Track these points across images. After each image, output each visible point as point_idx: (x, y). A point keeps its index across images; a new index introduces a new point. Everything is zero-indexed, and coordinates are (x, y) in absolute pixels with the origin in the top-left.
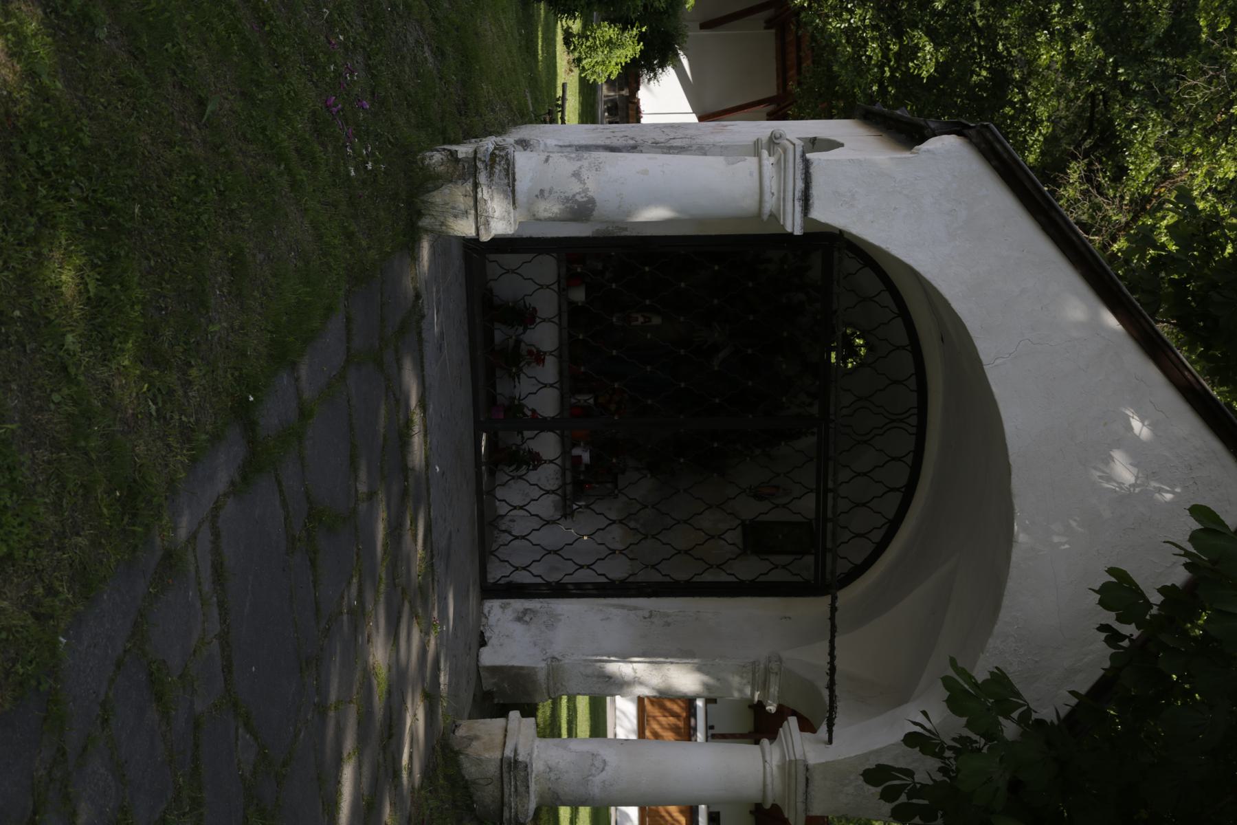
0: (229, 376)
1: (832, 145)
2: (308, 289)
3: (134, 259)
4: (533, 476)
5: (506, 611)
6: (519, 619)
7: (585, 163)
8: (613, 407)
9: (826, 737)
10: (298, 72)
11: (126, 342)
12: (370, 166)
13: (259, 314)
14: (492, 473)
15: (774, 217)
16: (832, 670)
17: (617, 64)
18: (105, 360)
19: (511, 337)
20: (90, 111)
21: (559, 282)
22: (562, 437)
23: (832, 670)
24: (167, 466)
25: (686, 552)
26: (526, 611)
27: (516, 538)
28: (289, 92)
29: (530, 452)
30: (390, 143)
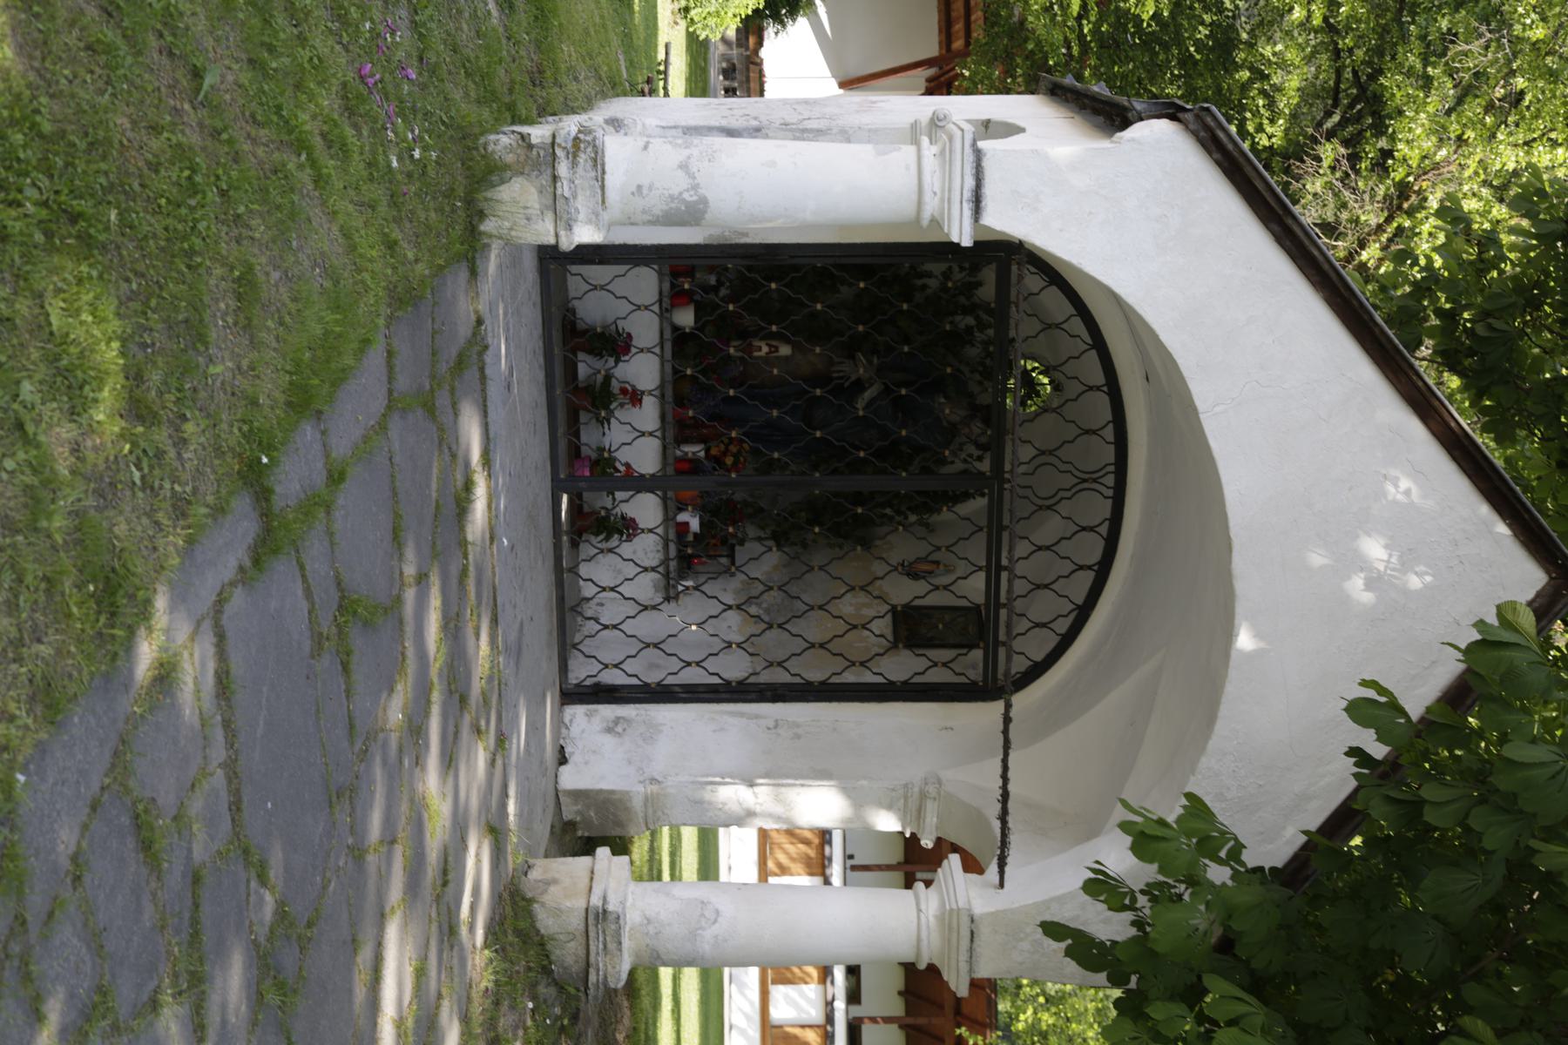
0: (236, 430)
1: (1010, 130)
2: (338, 316)
3: (110, 281)
4: (626, 549)
5: (593, 719)
6: (609, 730)
7: (695, 152)
8: (729, 461)
9: (996, 879)
10: (323, 32)
11: (100, 390)
12: (417, 154)
13: (275, 350)
14: (575, 545)
15: (936, 223)
16: (1005, 796)
17: (735, 16)
18: (73, 414)
19: (599, 372)
20: (50, 86)
21: (660, 301)
22: (664, 500)
23: (1005, 796)
24: (155, 549)
25: (822, 646)
26: (617, 720)
27: (606, 627)
28: (311, 59)
29: (623, 517)
30: (443, 123)
